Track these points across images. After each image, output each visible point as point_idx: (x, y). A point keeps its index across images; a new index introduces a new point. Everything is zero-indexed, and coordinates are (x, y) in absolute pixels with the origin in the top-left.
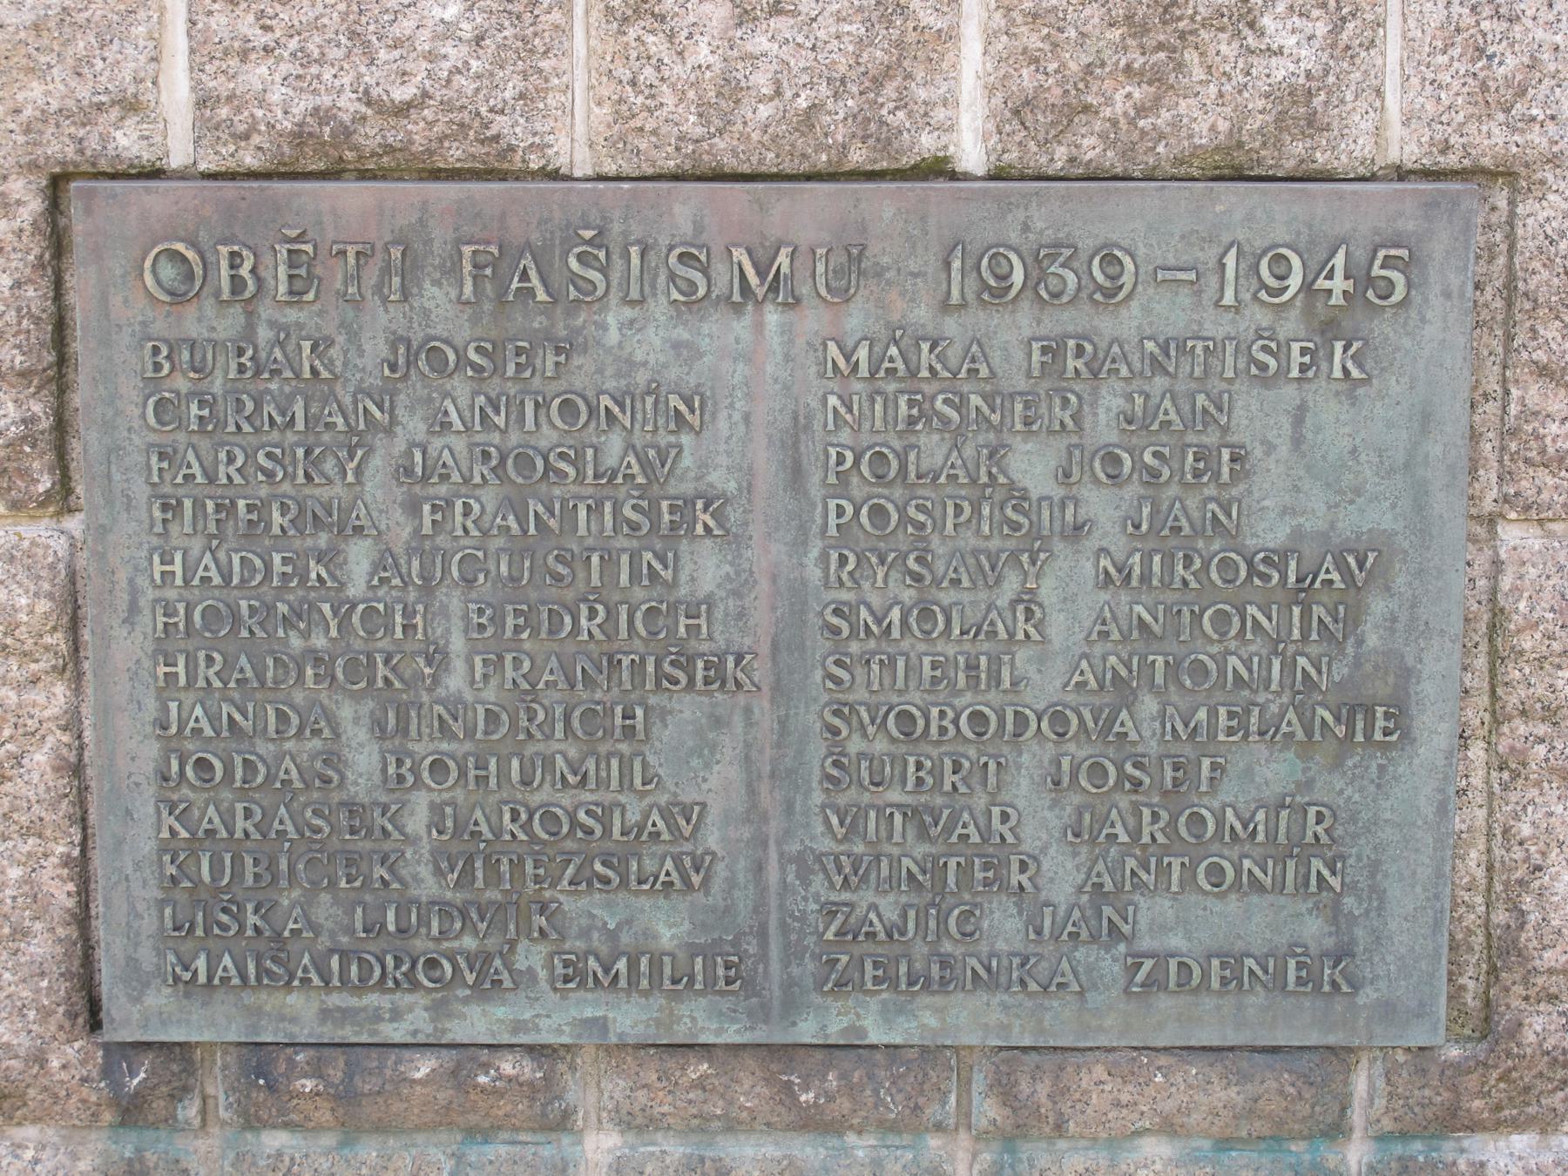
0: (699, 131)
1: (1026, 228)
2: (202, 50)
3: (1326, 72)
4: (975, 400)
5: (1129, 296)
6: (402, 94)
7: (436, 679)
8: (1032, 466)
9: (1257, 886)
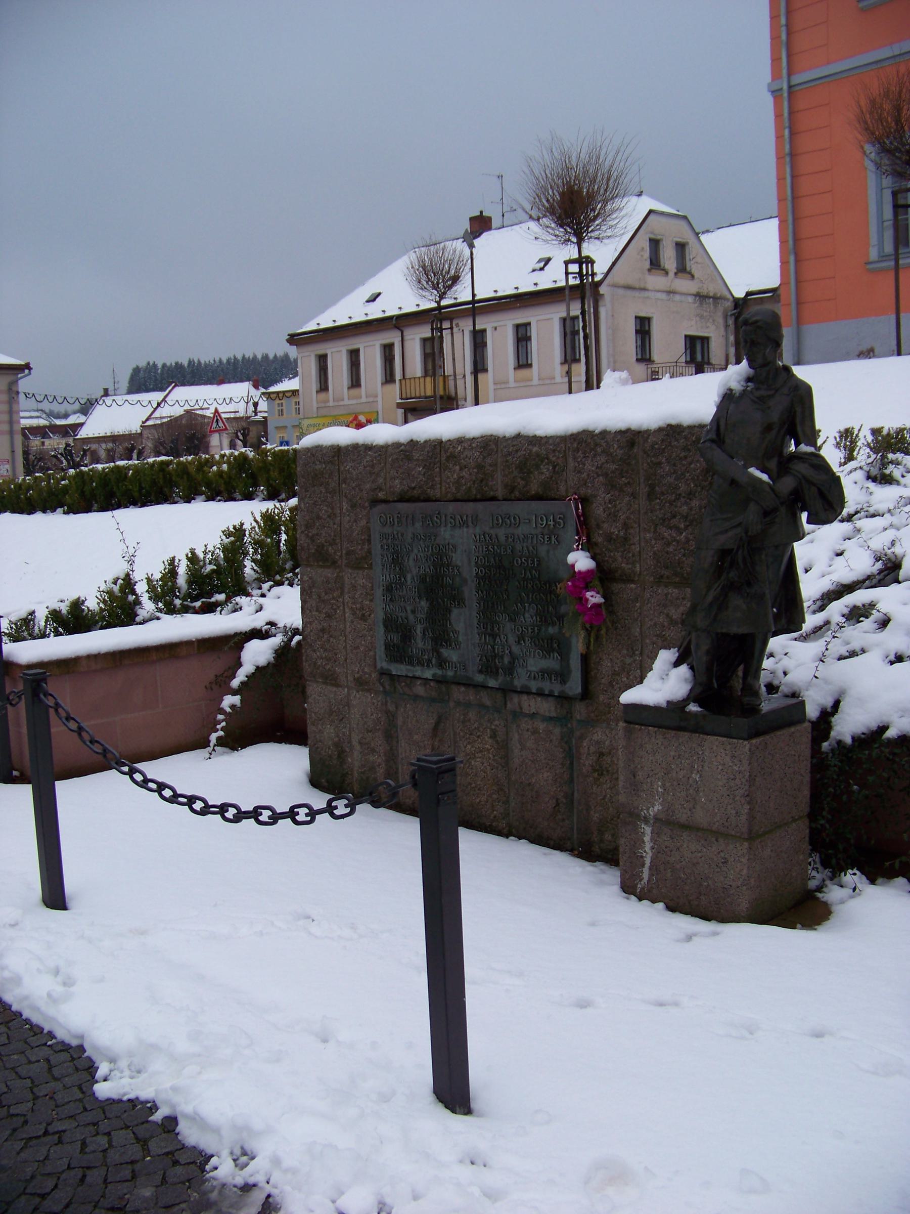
6: (413, 485)
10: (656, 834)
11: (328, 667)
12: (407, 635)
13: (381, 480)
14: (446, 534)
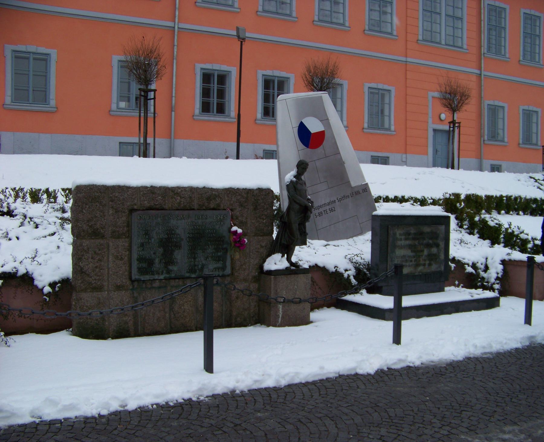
10: (283, 307)
11: (99, 283)
12: (151, 263)
13: (136, 201)
14: (173, 222)
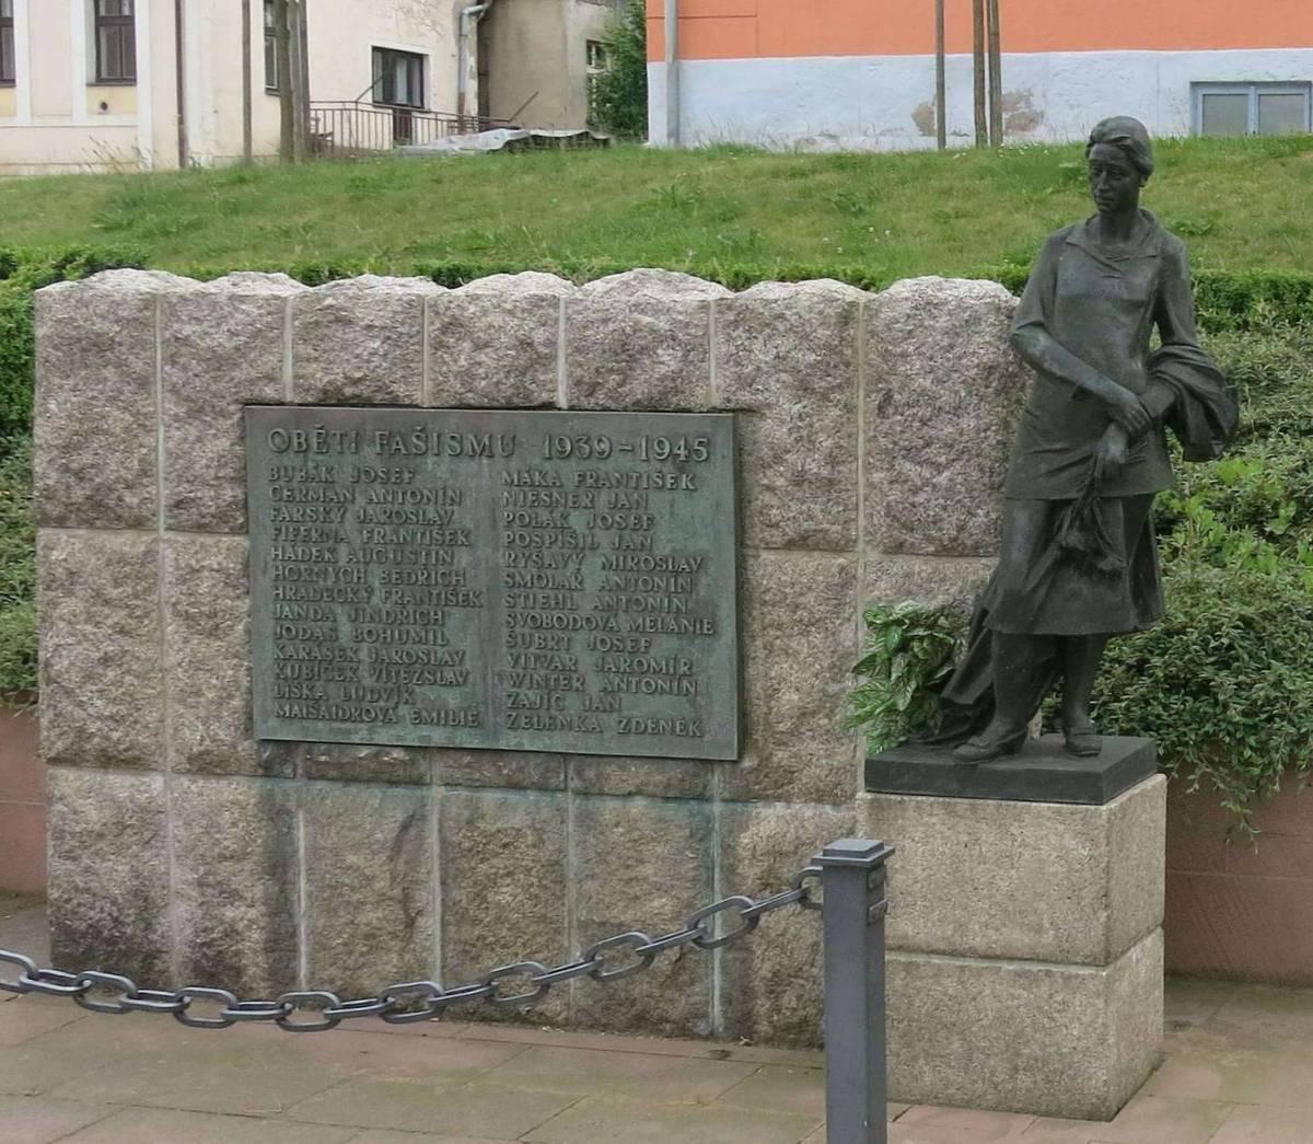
0: (462, 390)
1: (572, 428)
2: (297, 359)
3: (681, 371)
4: (555, 494)
5: (609, 455)
6: (358, 375)
7: (369, 598)
8: (577, 521)
9: (663, 691)
11: (115, 735)
